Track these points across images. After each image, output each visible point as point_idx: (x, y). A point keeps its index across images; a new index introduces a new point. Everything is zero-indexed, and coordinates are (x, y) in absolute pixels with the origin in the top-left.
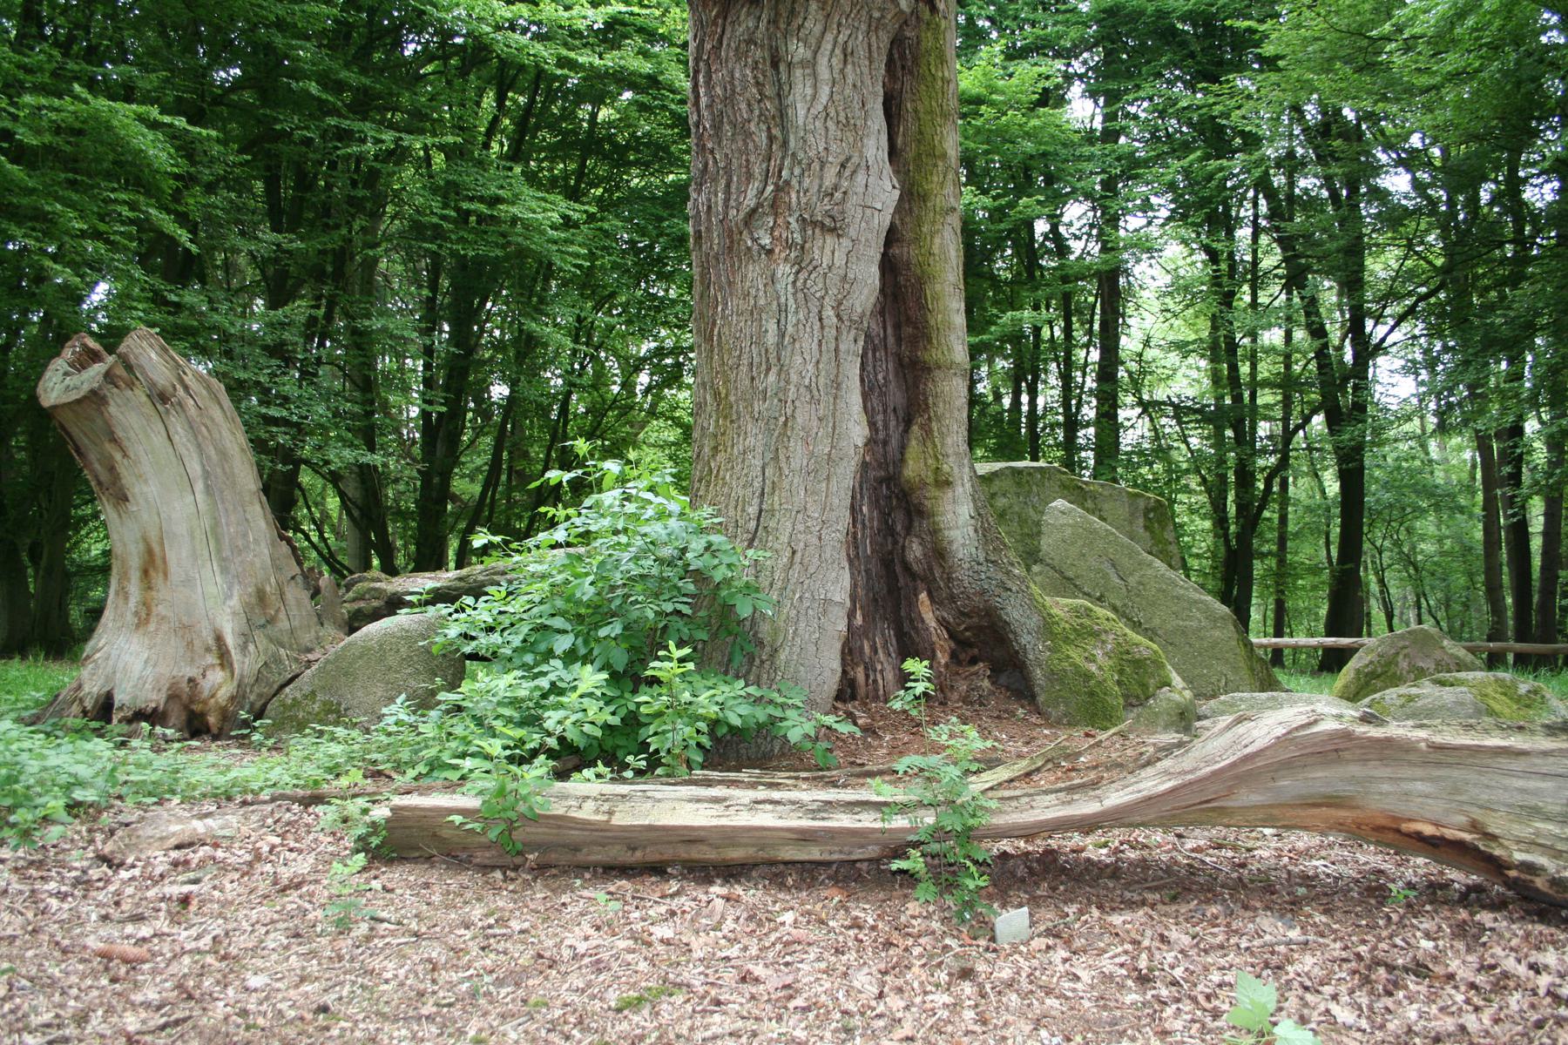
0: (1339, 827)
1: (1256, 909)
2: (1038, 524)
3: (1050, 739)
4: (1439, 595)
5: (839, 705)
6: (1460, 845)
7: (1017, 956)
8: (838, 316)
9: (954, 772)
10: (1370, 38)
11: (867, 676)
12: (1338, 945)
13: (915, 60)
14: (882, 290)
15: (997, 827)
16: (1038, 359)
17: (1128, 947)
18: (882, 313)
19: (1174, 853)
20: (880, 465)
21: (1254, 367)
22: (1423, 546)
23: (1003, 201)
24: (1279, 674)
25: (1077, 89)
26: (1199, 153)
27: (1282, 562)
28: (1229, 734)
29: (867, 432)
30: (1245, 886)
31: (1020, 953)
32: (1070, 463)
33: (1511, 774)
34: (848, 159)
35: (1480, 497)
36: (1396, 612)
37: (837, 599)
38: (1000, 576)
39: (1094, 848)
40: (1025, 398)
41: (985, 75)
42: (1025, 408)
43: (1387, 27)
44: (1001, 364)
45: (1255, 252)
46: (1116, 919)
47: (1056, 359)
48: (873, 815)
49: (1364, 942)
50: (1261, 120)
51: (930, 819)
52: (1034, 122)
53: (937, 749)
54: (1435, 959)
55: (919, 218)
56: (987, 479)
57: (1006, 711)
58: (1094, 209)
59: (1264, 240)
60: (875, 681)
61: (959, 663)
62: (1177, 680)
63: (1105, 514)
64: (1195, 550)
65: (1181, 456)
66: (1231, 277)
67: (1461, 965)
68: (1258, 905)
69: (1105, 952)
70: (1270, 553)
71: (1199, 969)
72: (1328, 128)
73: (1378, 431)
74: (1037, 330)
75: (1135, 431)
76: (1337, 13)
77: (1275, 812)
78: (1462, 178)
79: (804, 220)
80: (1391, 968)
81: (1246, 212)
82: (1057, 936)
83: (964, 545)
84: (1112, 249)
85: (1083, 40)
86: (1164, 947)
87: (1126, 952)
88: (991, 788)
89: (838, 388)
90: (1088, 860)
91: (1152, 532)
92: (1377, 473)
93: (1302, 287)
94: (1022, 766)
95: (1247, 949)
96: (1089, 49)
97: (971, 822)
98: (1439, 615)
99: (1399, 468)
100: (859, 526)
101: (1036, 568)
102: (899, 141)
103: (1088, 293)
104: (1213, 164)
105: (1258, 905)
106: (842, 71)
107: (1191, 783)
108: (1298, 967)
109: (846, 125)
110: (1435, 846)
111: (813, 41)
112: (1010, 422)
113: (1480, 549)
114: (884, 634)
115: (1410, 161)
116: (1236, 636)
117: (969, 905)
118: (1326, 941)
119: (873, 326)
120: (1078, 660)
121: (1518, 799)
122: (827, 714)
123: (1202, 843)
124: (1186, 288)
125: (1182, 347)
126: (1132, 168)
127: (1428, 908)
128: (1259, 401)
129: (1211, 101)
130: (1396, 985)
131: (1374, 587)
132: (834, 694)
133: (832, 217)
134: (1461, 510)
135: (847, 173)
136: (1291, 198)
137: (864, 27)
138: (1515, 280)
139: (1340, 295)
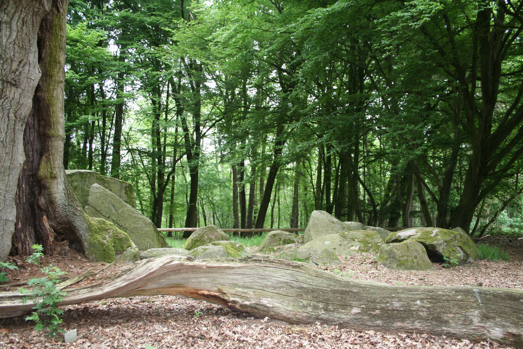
0: (180, 293)
1: (153, 322)
2: (88, 191)
3: (88, 267)
4: (220, 213)
5: (11, 257)
6: (215, 297)
7: (72, 347)
8: (15, 116)
9: (50, 284)
10: (205, 40)
11: (23, 246)
12: (179, 331)
13: (51, 28)
14: (33, 107)
15: (66, 301)
16: (93, 132)
17: (111, 339)
18: (33, 116)
19: (129, 305)
20: (30, 170)
21: (165, 139)
22: (215, 198)
23: (83, 77)
24: (168, 241)
25: (112, 42)
26: (151, 68)
27: (172, 203)
28: (145, 266)
29: (25, 159)
30: (150, 315)
31: (73, 345)
32: (103, 170)
33: (229, 274)
34: (22, 60)
35: (232, 183)
36: (207, 218)
37: (11, 219)
38: (73, 210)
39: (101, 305)
40: (88, 145)
41: (79, 32)
42: (88, 149)
43: (210, 37)
44: (80, 132)
45: (167, 102)
46: (107, 330)
47: (100, 133)
48: (20, 300)
49: (186, 330)
50: (171, 61)
51: (41, 301)
52: (96, 51)
53: (44, 275)
54: (207, 333)
55: (49, 83)
56: (71, 176)
57: (74, 257)
58: (115, 82)
59: (170, 99)
60: (26, 248)
61: (58, 241)
62: (133, 245)
63: (112, 188)
64: (144, 198)
65: (141, 167)
66: (159, 110)
67: (214, 335)
68: (154, 320)
69: (103, 342)
70: (168, 200)
71: (134, 344)
72: (192, 66)
73: (203, 162)
74: (94, 123)
75: (126, 158)
76: (196, 30)
77: (160, 290)
78: (230, 86)
79: (3, 80)
80: (193, 338)
81: (166, 88)
82: (87, 338)
83: (60, 199)
84: (120, 97)
85: (115, 25)
86: (123, 338)
87: (110, 341)
88: (64, 288)
89: (14, 142)
90: (99, 310)
91: (127, 195)
92: (202, 174)
93: (181, 115)
94: (76, 279)
95: (150, 336)
96: (117, 29)
97: (56, 301)
98: (220, 219)
99: (209, 173)
100: (21, 192)
101: (86, 207)
102: (43, 55)
103: (112, 110)
104: (155, 73)
105: (154, 320)
106: (22, 28)
107: (132, 283)
108: (166, 340)
109: (22, 48)
110: (208, 297)
111: (11, 15)
112: (83, 153)
113: (232, 199)
114: (30, 231)
115: (217, 79)
116: (153, 229)
117: (55, 330)
118: (175, 331)
119: (30, 120)
120: (100, 239)
121: (231, 282)
122: (5, 262)
123: (138, 301)
124: (144, 112)
125: (142, 132)
126: (129, 70)
127: (206, 317)
128: (167, 150)
129: (156, 52)
130: (195, 343)
131: (201, 210)
132: (8, 254)
133: (15, 81)
134: (227, 187)
135: (22, 65)
136: (179, 86)
137: (31, 13)
138: (244, 118)
139: (193, 118)
